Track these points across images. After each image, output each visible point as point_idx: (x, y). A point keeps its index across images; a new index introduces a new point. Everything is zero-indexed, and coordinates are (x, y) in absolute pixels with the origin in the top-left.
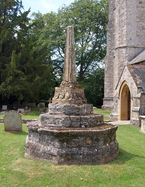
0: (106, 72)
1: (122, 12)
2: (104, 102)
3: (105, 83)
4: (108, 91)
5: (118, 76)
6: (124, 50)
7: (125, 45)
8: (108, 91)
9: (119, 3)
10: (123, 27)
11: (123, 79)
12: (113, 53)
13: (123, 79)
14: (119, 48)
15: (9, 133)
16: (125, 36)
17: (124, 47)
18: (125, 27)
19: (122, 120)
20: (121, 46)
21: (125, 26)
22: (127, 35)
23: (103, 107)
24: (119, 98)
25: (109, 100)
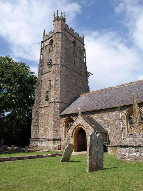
0: (33, 118)
1: (57, 79)
2: (31, 142)
3: (32, 127)
4: (34, 133)
5: (53, 122)
6: (58, 104)
7: (59, 101)
8: (34, 133)
9: (55, 72)
10: (58, 88)
11: (77, 123)
12: (39, 104)
13: (77, 123)
14: (55, 102)
15: (64, 162)
16: (59, 95)
17: (58, 102)
18: (59, 89)
19: (75, 152)
20: (56, 101)
21: (59, 88)
22: (60, 94)
23: (30, 146)
24: (72, 137)
25: (35, 140)
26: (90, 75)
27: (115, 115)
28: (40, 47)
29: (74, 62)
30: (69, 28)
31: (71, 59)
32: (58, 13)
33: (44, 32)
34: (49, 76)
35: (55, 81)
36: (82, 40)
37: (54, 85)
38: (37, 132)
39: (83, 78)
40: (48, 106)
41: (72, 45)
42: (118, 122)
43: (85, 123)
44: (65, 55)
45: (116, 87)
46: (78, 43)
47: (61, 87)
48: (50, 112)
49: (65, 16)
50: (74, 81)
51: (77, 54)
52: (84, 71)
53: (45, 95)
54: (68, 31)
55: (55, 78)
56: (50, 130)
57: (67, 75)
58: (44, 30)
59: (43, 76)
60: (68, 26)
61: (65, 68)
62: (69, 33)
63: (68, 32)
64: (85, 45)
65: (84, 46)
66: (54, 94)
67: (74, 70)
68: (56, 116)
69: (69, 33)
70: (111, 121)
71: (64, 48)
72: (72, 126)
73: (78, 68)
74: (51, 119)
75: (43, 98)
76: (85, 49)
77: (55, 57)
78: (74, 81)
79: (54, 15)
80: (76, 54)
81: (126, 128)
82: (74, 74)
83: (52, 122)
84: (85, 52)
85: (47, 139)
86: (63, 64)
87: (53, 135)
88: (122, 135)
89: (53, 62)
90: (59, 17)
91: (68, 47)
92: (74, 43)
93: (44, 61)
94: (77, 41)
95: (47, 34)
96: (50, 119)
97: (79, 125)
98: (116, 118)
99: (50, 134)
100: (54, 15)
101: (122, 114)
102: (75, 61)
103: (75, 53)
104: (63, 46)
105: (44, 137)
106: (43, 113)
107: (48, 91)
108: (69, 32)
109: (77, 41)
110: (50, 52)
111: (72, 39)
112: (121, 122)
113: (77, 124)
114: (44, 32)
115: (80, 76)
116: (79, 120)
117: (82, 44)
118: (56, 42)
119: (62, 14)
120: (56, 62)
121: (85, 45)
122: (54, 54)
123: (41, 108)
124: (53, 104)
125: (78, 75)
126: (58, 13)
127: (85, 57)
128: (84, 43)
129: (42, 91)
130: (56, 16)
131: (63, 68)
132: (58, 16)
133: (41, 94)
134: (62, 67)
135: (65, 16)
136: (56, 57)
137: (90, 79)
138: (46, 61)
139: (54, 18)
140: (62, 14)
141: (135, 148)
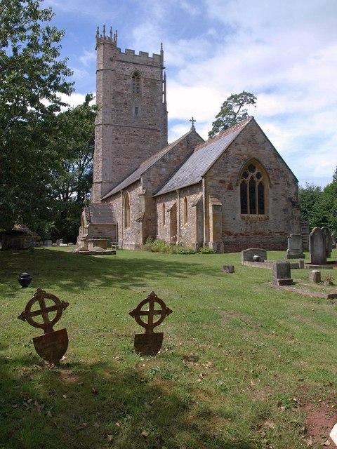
7: (100, 180)
18: (101, 163)
30: (123, 51)
32: (104, 31)
44: (113, 106)
46: (146, 72)
47: (104, 160)
50: (133, 145)
57: (117, 139)
61: (113, 127)
65: (164, 70)
76: (165, 77)
78: (133, 145)
86: (107, 122)
91: (120, 88)
94: (138, 68)
111: (130, 69)
119: (111, 33)
121: (164, 68)
126: (104, 31)
127: (165, 93)
131: (109, 129)
134: (105, 128)
137: (300, 184)
140: (111, 33)
141: (276, 258)
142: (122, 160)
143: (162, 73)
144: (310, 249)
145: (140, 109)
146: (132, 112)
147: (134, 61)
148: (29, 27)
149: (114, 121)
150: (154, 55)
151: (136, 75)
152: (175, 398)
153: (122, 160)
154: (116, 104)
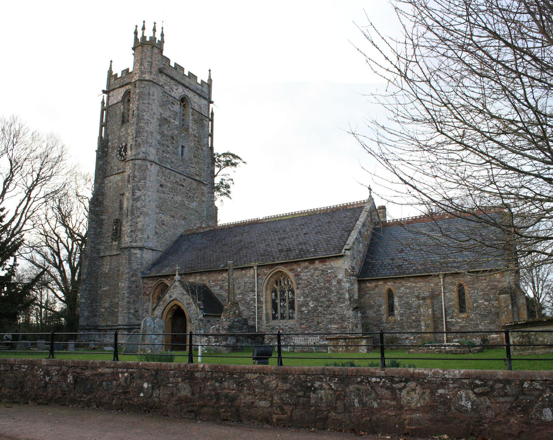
5: (128, 291)
9: (133, 180)
11: (171, 297)
13: (171, 297)
26: (241, 164)
27: (246, 283)
28: (100, 106)
29: (182, 151)
31: (172, 143)
32: (144, 28)
33: (111, 68)
34: (120, 184)
35: (134, 200)
36: (205, 90)
37: (130, 208)
38: (94, 313)
39: (203, 187)
40: (117, 255)
41: (177, 107)
42: (251, 295)
43: (185, 297)
44: (159, 137)
45: (266, 219)
48: (121, 269)
49: (162, 35)
50: (178, 198)
51: (191, 130)
52: (207, 171)
53: (111, 230)
54: (169, 72)
55: (133, 194)
56: (120, 309)
57: (161, 186)
58: (111, 62)
59: (106, 182)
60: (168, 60)
61: (158, 167)
62: (172, 79)
63: (167, 75)
64: (212, 102)
65: (211, 105)
66: (129, 231)
67: (181, 169)
68: (134, 279)
69: (172, 79)
70: (239, 294)
71: (156, 120)
72: (161, 303)
73: (192, 163)
74: (123, 285)
75: (106, 235)
76: (212, 114)
77: (134, 143)
78: (178, 198)
79: (136, 33)
80: (187, 130)
81: (264, 307)
82: (178, 180)
83: (125, 292)
84: (212, 120)
85: (525, 358)
87: (126, 320)
88: (257, 320)
89: (129, 152)
90: (148, 39)
91: (167, 114)
92: (184, 100)
93: (110, 144)
94: (190, 95)
95: (116, 75)
96: (121, 285)
97: (174, 300)
98: (249, 288)
99: (120, 318)
100: (136, 33)
101: (260, 281)
102: (183, 147)
103: (184, 127)
104: (154, 114)
105: (109, 323)
106: (107, 271)
107: (117, 220)
108: (170, 77)
109: (190, 95)
110: (123, 122)
111: (178, 92)
112: (256, 297)
113: (171, 299)
114: (111, 68)
115: (194, 182)
116: (175, 290)
117: (206, 102)
118: (136, 103)
119: (154, 30)
120: (135, 155)
121: (212, 102)
122: (133, 135)
123: (102, 257)
124: (128, 253)
125: (190, 180)
126: (144, 28)
127: (211, 135)
128: (210, 98)
129: (104, 217)
130: (139, 36)
132: (144, 38)
133: (102, 224)
135: (162, 35)
136: (136, 141)
138: (114, 143)
139: (136, 39)
140: (154, 30)
142: (166, 218)
143: (209, 109)
144: (256, 290)
145: (186, 150)
146: (178, 151)
147: (183, 82)
148: (448, 34)
149: (159, 159)
150: (202, 81)
151: (184, 100)
152: (68, 225)
153: (166, 218)
154: (162, 134)
